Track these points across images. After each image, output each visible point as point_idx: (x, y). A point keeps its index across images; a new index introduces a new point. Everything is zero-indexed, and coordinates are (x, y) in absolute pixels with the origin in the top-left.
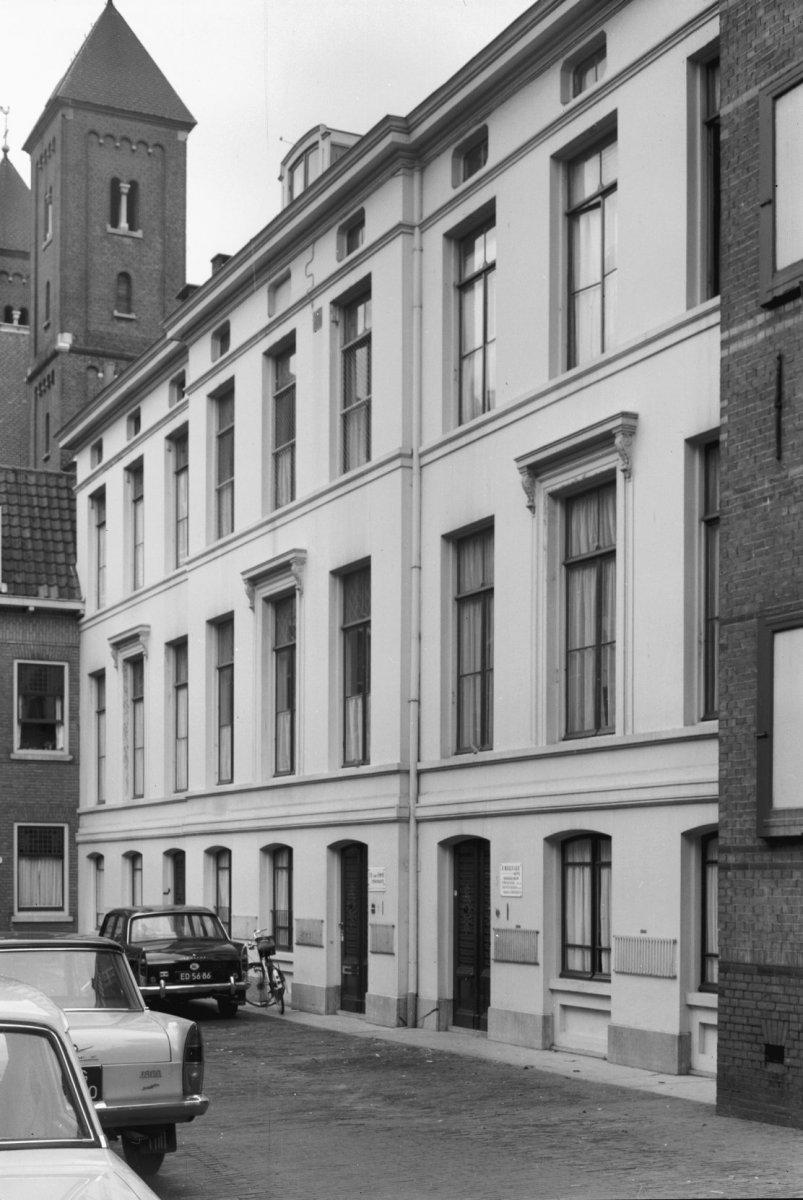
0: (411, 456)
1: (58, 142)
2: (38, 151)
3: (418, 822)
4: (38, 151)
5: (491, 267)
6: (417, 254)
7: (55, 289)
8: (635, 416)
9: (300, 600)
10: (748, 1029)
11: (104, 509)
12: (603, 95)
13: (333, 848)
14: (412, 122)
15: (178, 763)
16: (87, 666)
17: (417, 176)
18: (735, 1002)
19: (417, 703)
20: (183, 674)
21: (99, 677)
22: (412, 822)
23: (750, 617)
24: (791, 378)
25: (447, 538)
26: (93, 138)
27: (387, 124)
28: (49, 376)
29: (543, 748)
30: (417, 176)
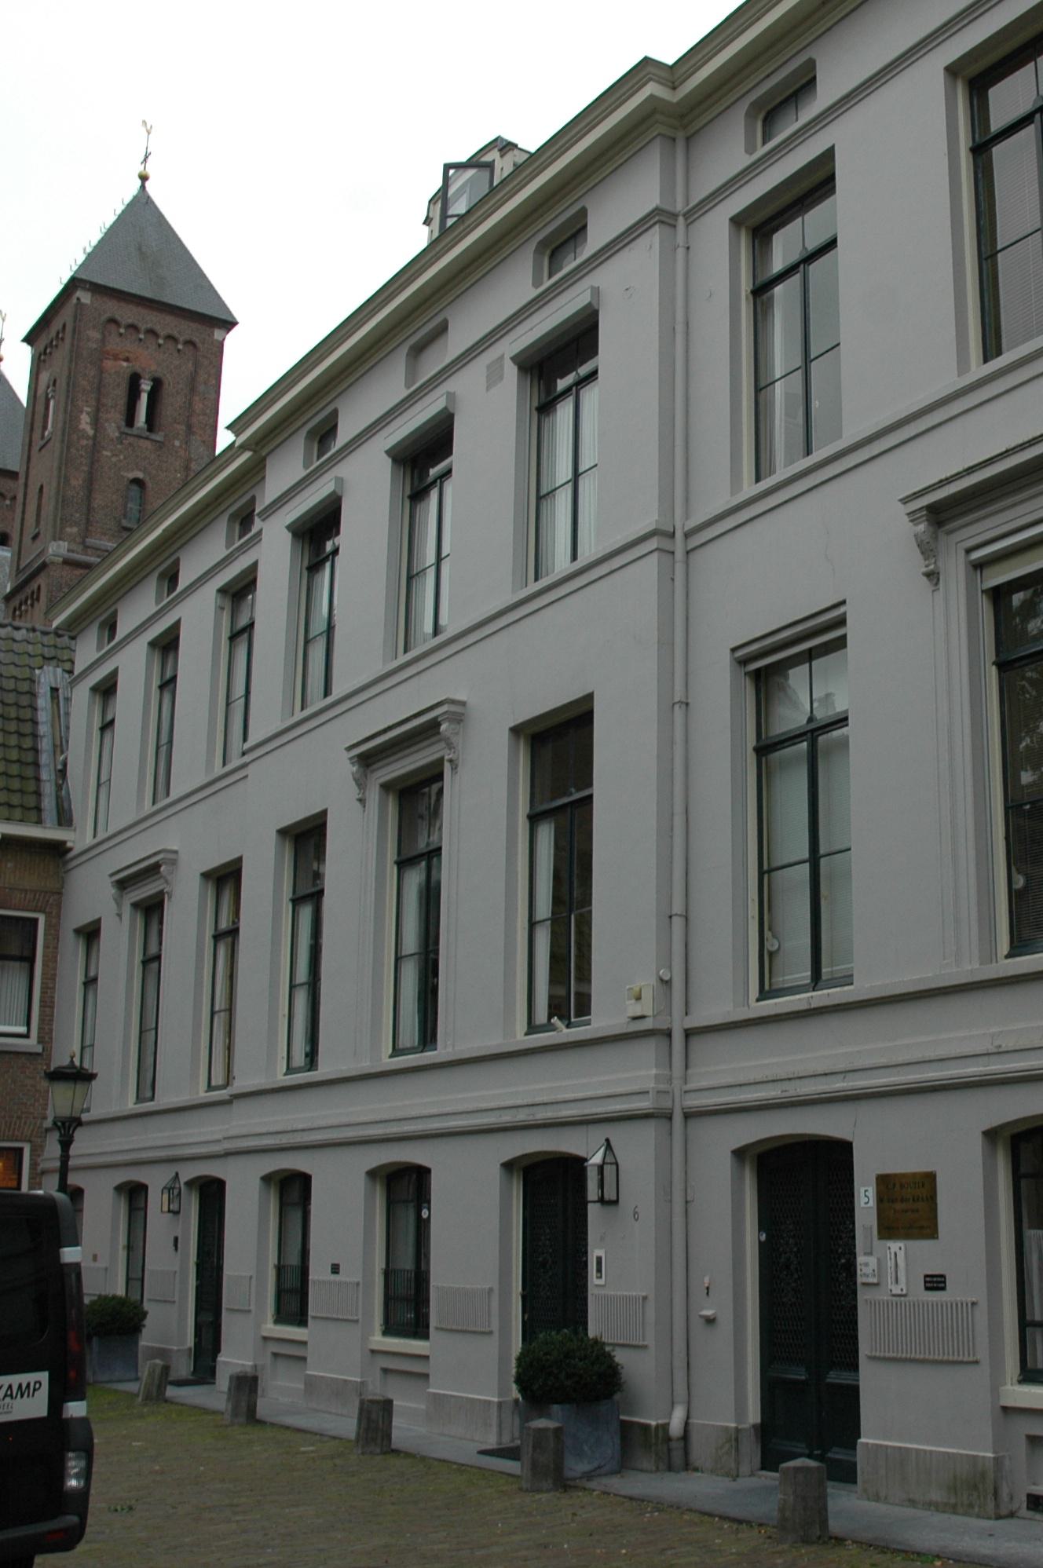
0: (672, 535)
1: (69, 329)
2: (43, 341)
3: (688, 1116)
6: (681, 252)
7: (50, 492)
15: (930, 1282)
16: (78, 914)
17: (680, 145)
19: (683, 919)
20: (434, 872)
21: (91, 934)
22: (678, 1118)
25: (206, 876)
26: (113, 327)
27: (646, 67)
28: (33, 593)
29: (971, 969)
30: (680, 145)
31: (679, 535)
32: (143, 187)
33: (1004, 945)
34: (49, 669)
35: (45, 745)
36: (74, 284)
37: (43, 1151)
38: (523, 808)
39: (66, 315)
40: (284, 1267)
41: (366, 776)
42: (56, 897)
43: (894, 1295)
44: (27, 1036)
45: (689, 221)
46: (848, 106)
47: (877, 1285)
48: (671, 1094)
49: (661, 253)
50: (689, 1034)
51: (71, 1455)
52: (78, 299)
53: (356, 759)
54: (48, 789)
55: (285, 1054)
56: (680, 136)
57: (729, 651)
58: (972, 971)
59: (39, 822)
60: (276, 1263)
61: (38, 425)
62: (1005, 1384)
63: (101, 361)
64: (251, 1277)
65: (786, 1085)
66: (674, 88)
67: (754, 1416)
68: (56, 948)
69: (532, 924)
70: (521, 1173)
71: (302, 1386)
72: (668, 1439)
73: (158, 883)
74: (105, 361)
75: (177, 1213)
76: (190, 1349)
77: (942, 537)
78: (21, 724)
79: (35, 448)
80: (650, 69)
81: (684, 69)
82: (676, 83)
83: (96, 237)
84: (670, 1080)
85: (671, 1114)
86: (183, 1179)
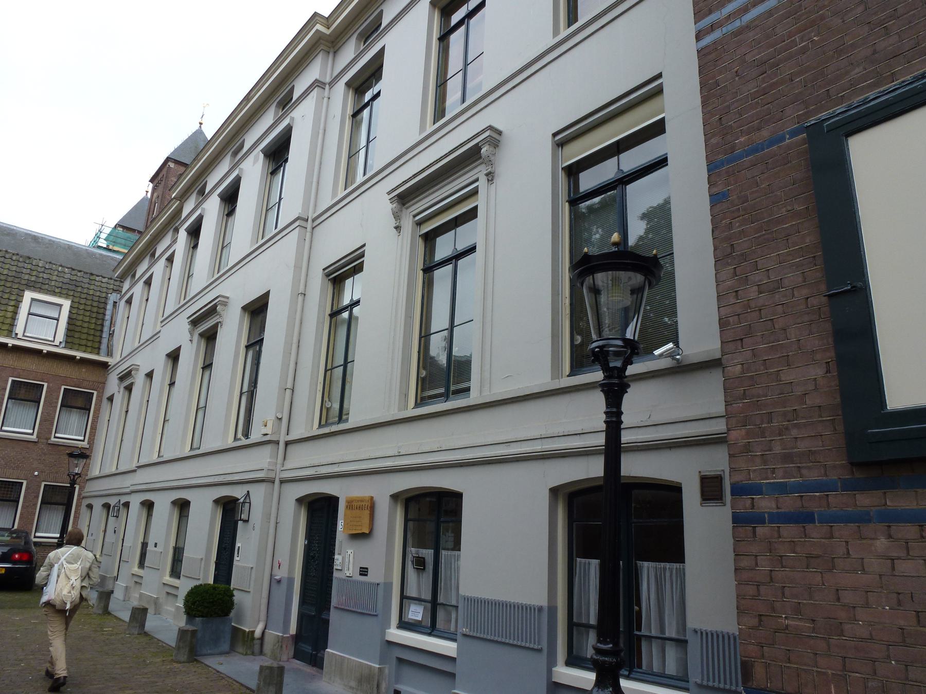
2: (156, 181)
3: (282, 482)
6: (326, 99)
8: (500, 133)
9: (220, 330)
13: (217, 501)
14: (331, 20)
17: (331, 55)
21: (111, 399)
30: (331, 55)
31: (310, 220)
32: (200, 127)
34: (114, 294)
35: (107, 324)
36: (168, 159)
38: (244, 342)
39: (164, 172)
41: (194, 330)
43: (347, 576)
44: (32, 434)
45: (331, 86)
46: (392, 26)
47: (341, 570)
48: (275, 472)
50: (287, 444)
51: (599, 561)
52: (169, 165)
54: (105, 341)
55: (158, 450)
58: (393, 414)
59: (98, 354)
61: (151, 213)
64: (202, 559)
66: (328, 28)
67: (293, 630)
69: (241, 394)
70: (222, 506)
71: (138, 596)
72: (253, 639)
76: (115, 577)
77: (404, 210)
80: (317, 18)
81: (332, 19)
83: (179, 143)
84: (276, 464)
86: (121, 503)
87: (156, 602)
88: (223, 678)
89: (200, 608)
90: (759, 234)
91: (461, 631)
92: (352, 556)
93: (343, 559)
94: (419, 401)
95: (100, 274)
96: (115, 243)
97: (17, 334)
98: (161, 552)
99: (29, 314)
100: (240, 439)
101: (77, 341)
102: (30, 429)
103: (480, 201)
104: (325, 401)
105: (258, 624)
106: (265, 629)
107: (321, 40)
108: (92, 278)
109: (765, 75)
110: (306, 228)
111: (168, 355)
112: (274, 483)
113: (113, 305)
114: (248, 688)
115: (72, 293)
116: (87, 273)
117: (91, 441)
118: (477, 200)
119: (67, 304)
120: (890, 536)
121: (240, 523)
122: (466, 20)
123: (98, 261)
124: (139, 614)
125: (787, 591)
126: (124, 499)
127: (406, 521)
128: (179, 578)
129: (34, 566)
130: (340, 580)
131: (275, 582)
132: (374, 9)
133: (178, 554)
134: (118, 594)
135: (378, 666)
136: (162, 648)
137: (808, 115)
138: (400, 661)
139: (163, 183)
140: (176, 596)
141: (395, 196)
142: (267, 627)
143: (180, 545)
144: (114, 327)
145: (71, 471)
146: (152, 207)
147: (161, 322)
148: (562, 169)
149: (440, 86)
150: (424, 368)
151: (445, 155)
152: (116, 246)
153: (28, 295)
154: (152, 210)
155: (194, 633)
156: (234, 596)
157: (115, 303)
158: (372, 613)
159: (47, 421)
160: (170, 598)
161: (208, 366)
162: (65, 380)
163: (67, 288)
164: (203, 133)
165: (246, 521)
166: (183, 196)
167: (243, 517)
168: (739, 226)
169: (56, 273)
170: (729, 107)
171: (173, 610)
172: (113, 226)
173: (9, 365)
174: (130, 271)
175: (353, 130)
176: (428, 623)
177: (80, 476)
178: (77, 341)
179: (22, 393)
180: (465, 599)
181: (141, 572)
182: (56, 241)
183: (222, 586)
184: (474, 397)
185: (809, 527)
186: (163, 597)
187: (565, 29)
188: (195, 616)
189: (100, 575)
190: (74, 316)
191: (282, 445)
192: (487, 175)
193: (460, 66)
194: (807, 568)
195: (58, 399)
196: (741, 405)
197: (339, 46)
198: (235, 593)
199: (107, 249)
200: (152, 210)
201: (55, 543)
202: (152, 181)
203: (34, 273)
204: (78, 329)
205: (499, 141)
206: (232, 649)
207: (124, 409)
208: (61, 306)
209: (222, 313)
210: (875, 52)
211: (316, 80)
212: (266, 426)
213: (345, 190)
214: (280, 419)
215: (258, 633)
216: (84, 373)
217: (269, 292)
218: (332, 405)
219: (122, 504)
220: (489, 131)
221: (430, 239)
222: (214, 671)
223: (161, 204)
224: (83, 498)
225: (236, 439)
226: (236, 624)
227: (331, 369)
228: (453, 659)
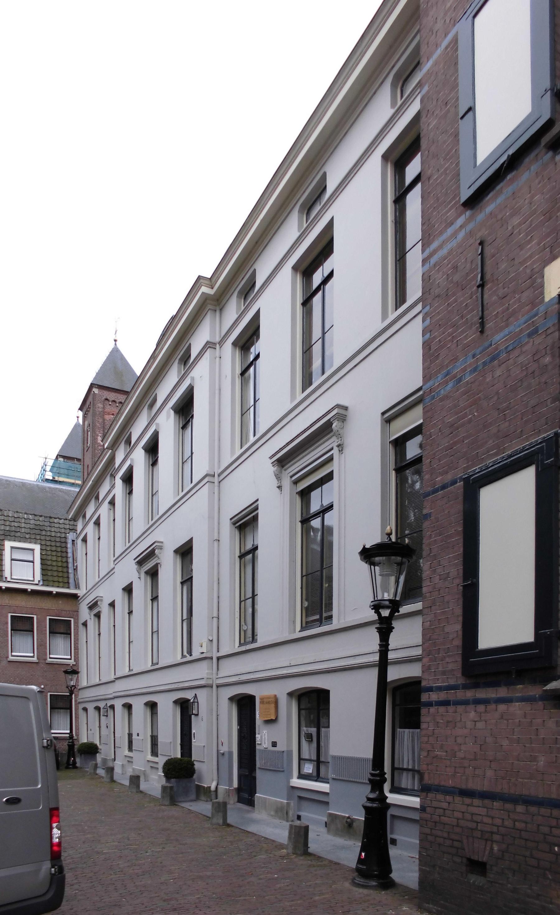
0: (214, 476)
2: (85, 409)
3: (218, 686)
4: (85, 409)
5: (257, 357)
6: (218, 359)
8: (346, 408)
10: (448, 842)
11: (213, 644)
12: (323, 212)
13: (176, 702)
14: (213, 280)
18: (436, 818)
21: (85, 624)
22: (214, 687)
23: (454, 482)
24: (493, 256)
26: (107, 402)
31: (216, 475)
32: (116, 344)
33: (298, 627)
35: (70, 560)
36: (92, 386)
37: (78, 696)
38: (179, 580)
39: (90, 399)
40: (154, 736)
42: (76, 612)
43: (265, 748)
44: (33, 657)
47: (261, 744)
49: (210, 360)
50: (218, 659)
52: (94, 392)
53: (136, 563)
54: (71, 576)
56: (218, 309)
57: (229, 520)
59: (68, 588)
60: (151, 734)
61: (86, 442)
62: (292, 778)
63: (104, 415)
64: (171, 742)
65: (239, 676)
66: (212, 288)
67: (235, 784)
68: (78, 630)
69: (183, 621)
71: (132, 770)
72: (210, 791)
73: (98, 608)
74: (105, 416)
75: (107, 716)
78: (62, 553)
79: (85, 451)
80: (201, 281)
82: (213, 285)
84: (212, 674)
85: (213, 686)
87: (144, 773)
88: (192, 813)
89: (173, 773)
90: (442, 543)
91: (331, 776)
92: (266, 734)
93: (261, 737)
94: (304, 625)
95: (56, 517)
96: (59, 474)
97: (6, 578)
98: (143, 740)
99: (12, 560)
100: (185, 657)
101: (51, 578)
102: (31, 653)
103: (335, 466)
104: (242, 625)
105: (212, 782)
106: (218, 785)
107: (207, 301)
108: (51, 520)
109: (452, 434)
110: (214, 483)
111: (124, 589)
112: (212, 687)
113: (72, 543)
114: (208, 817)
115: (38, 537)
116: (47, 517)
117: (77, 659)
118: (333, 466)
119: (37, 548)
120: (475, 711)
121: (193, 716)
122: (322, 287)
123: (49, 495)
124: (135, 780)
125: (439, 739)
126: (110, 703)
127: (300, 710)
128: (157, 756)
129: (57, 753)
130: (260, 750)
131: (220, 755)
132: (248, 268)
133: (154, 740)
134: (118, 770)
135: (286, 801)
136: (153, 799)
137: (468, 467)
138: (300, 798)
139: (91, 411)
140: (158, 768)
141: (275, 461)
142: (219, 784)
143: (155, 734)
144: (76, 563)
145: (68, 684)
146: (86, 435)
147: (114, 561)
148: (390, 442)
149: (305, 353)
150: (307, 600)
151: (307, 428)
152: (61, 476)
153: (8, 544)
154: (86, 439)
155: (171, 788)
156: (194, 765)
157: (73, 541)
158: (281, 770)
159: (42, 645)
160: (154, 770)
161: (155, 599)
162: (48, 612)
163: (34, 533)
164: (119, 350)
165: (197, 715)
166: (114, 446)
167: (194, 712)
168: (435, 537)
169: (23, 521)
170: (434, 454)
171: (157, 778)
172: (54, 457)
173: (6, 604)
174: (81, 512)
175: (243, 384)
176: (315, 774)
177: (75, 688)
178: (51, 578)
179: (20, 626)
180: (332, 757)
181: (130, 754)
182: (12, 481)
183: (186, 759)
184: (336, 624)
185: (449, 707)
186: (148, 770)
187: (392, 313)
188: (171, 778)
189: (102, 758)
190: (45, 557)
191: (215, 660)
192: (338, 446)
193: (320, 335)
194: (447, 727)
195: (46, 627)
196: (428, 644)
197: (223, 304)
198: (195, 763)
199: (54, 481)
200: (86, 439)
201: (67, 737)
202: (81, 409)
203: (8, 523)
204: (50, 568)
205: (346, 416)
206: (197, 799)
207: (97, 633)
208: (33, 550)
209: (159, 556)
210: (499, 431)
211: (207, 342)
212: (202, 646)
213: (241, 448)
214: (212, 641)
215: (213, 788)
216: (60, 604)
217: (192, 539)
218: (247, 628)
219: (109, 707)
220: (337, 409)
221: (305, 494)
222: (187, 809)
223: (93, 433)
224: (79, 703)
225: (183, 656)
226: (198, 782)
227: (245, 600)
228: (327, 794)
